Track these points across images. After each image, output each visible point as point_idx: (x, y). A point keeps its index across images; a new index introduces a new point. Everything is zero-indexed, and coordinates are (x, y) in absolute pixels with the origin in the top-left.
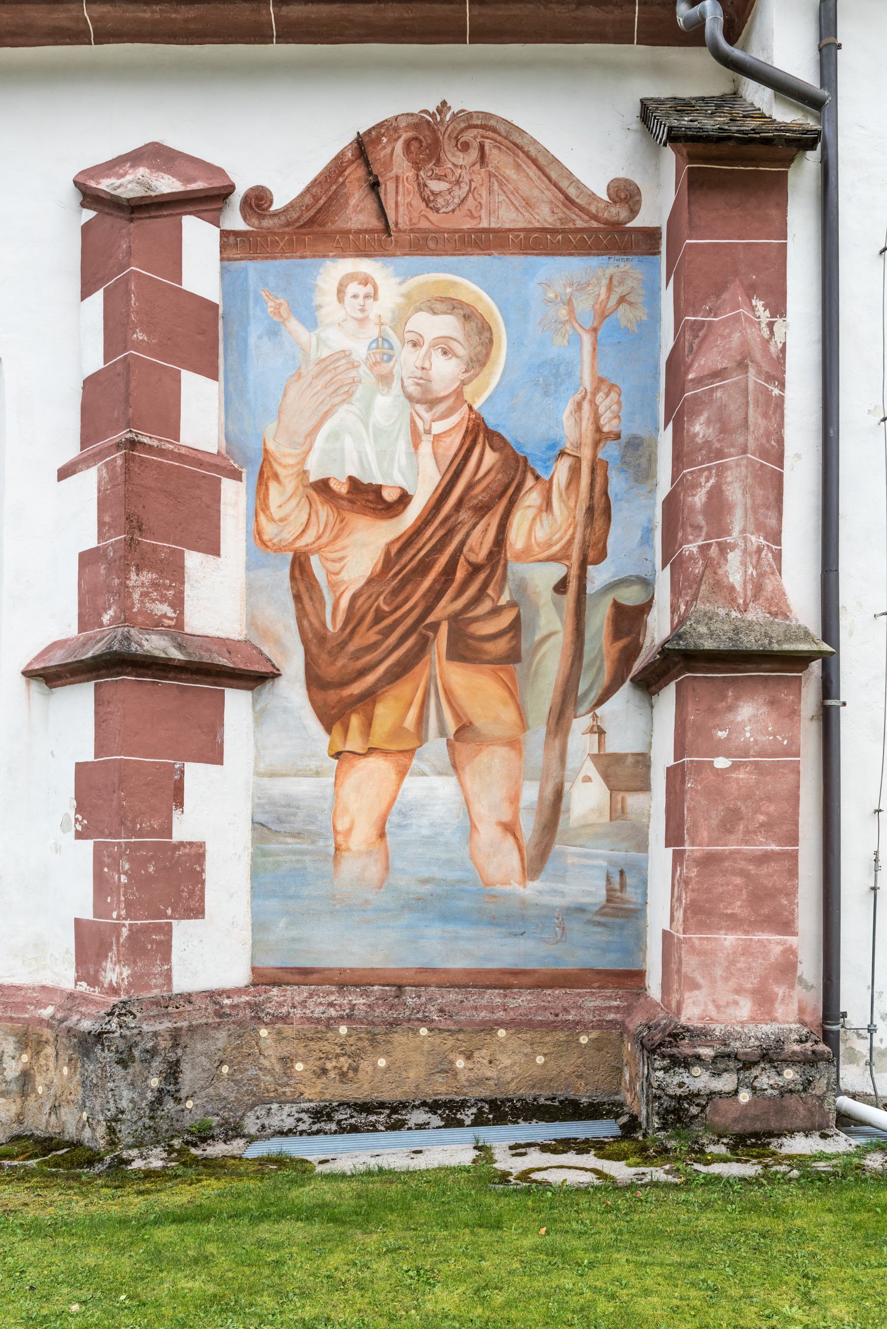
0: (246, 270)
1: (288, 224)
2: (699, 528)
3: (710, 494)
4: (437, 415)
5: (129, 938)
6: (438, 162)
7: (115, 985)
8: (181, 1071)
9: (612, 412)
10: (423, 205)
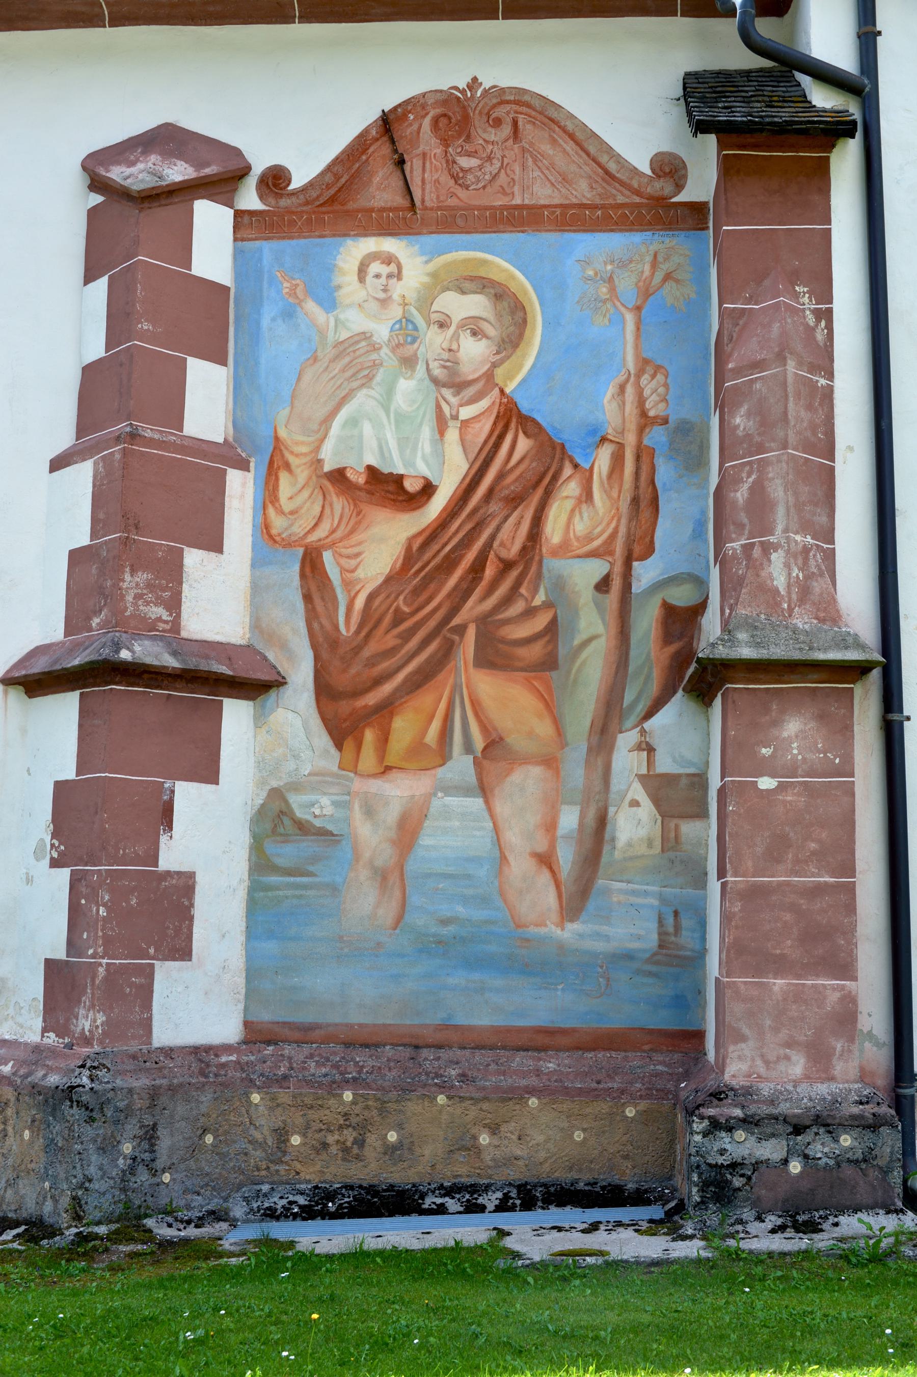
0: (260, 250)
1: (307, 203)
2: (743, 526)
3: (751, 489)
4: (465, 399)
5: (106, 979)
6: (468, 138)
7: (87, 1033)
8: (158, 1138)
9: (659, 395)
10: (452, 182)
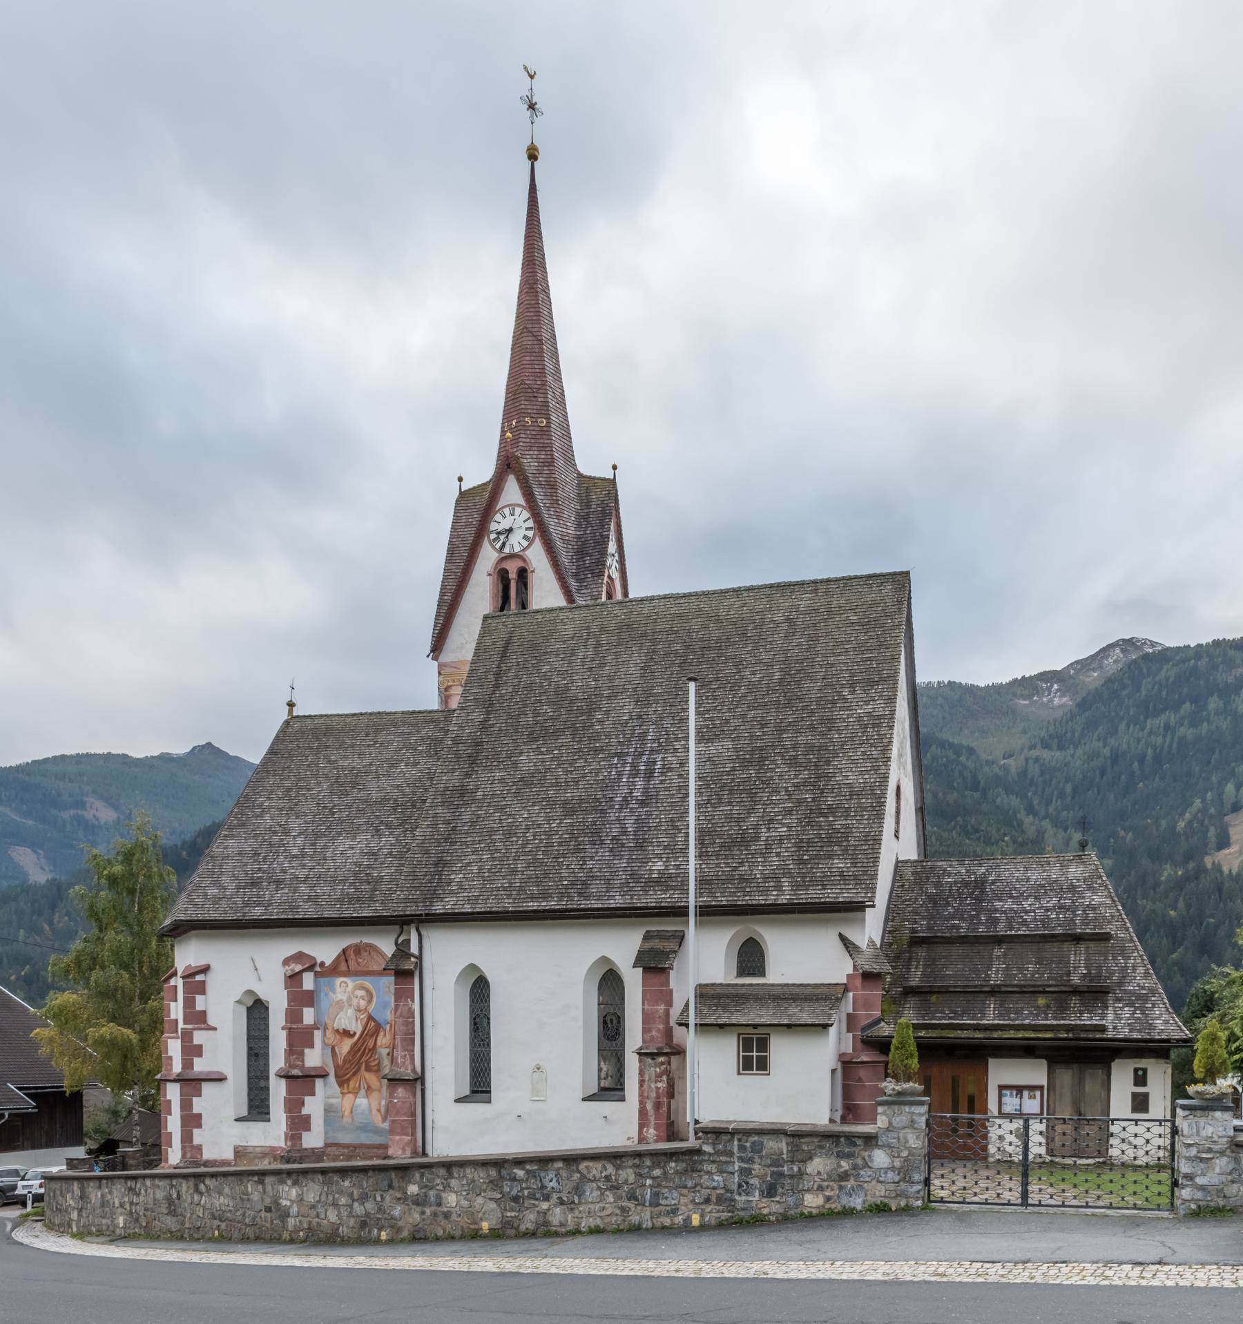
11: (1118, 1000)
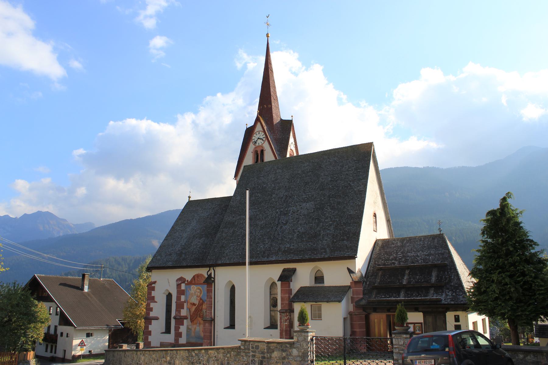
0: (251, 335)
11: (448, 289)
